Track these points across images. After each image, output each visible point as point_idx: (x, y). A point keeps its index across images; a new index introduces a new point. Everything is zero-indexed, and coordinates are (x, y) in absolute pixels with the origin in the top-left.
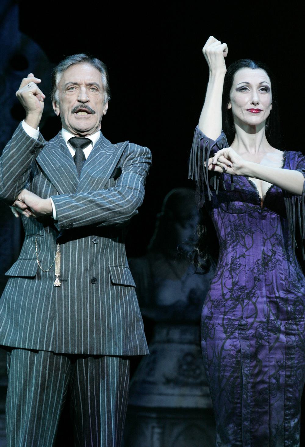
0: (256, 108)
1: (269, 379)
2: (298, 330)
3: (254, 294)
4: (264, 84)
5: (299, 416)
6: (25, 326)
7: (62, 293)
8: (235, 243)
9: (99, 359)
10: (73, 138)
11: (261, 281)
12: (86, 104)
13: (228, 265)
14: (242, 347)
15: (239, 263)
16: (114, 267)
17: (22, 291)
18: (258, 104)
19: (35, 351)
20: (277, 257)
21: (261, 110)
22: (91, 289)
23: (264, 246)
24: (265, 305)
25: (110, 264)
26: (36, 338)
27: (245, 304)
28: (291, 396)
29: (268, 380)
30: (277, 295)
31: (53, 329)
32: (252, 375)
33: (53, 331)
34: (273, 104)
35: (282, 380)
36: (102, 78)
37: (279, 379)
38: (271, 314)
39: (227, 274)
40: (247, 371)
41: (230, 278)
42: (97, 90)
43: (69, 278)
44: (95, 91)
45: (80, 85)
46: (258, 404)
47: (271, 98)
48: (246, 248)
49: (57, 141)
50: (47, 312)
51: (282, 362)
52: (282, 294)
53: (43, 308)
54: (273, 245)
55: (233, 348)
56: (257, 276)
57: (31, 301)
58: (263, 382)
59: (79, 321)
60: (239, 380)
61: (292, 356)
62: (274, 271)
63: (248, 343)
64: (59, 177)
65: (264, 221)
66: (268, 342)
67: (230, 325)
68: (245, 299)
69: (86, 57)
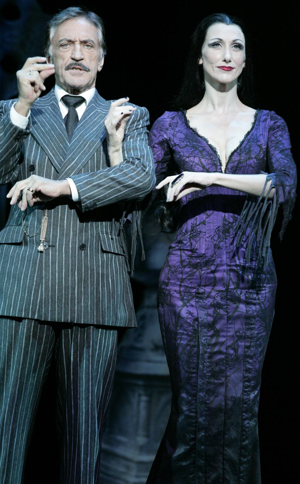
0: (227, 65)
1: (226, 349)
2: (259, 299)
4: (238, 42)
5: (259, 388)
6: (10, 294)
7: (49, 259)
9: (84, 328)
10: (66, 96)
14: (199, 316)
17: (8, 258)
18: (230, 61)
19: (19, 320)
21: (233, 68)
22: (80, 255)
24: (225, 274)
26: (21, 305)
28: (251, 367)
29: (225, 351)
30: (238, 263)
31: (39, 296)
32: (209, 345)
33: (39, 299)
34: (247, 61)
35: (240, 351)
36: (98, 34)
37: (238, 350)
38: (231, 283)
40: (204, 340)
42: (92, 47)
43: (57, 244)
44: (90, 48)
46: (215, 375)
47: (245, 55)
49: (49, 99)
50: (33, 279)
51: (241, 332)
55: (190, 316)
57: (17, 267)
58: (220, 352)
59: (67, 288)
60: (195, 349)
61: (252, 326)
63: (206, 312)
66: (227, 312)
67: (187, 292)
69: (81, 11)
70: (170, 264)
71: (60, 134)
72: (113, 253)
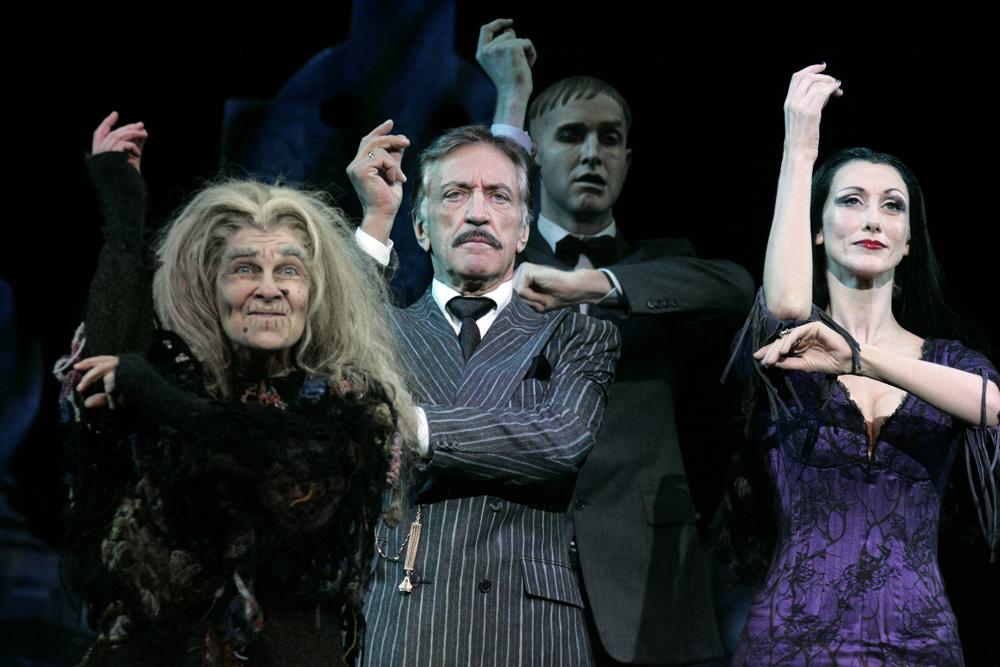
3: (835, 633)
4: (894, 193)
8: (808, 526)
11: (852, 609)
12: (484, 228)
13: (788, 570)
15: (810, 568)
16: (533, 563)
20: (891, 562)
22: (479, 603)
23: (867, 538)
25: (525, 556)
27: (813, 653)
30: (884, 638)
39: (783, 588)
41: (790, 597)
42: (507, 199)
43: (436, 578)
45: (474, 187)
48: (830, 539)
52: (893, 638)
53: (384, 639)
54: (885, 539)
56: (845, 598)
62: (883, 590)
64: (428, 376)
65: (872, 486)
68: (814, 642)
70: (751, 634)
71: (451, 363)
72: (541, 598)
